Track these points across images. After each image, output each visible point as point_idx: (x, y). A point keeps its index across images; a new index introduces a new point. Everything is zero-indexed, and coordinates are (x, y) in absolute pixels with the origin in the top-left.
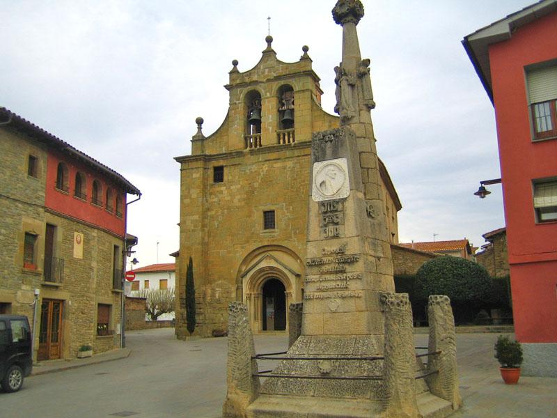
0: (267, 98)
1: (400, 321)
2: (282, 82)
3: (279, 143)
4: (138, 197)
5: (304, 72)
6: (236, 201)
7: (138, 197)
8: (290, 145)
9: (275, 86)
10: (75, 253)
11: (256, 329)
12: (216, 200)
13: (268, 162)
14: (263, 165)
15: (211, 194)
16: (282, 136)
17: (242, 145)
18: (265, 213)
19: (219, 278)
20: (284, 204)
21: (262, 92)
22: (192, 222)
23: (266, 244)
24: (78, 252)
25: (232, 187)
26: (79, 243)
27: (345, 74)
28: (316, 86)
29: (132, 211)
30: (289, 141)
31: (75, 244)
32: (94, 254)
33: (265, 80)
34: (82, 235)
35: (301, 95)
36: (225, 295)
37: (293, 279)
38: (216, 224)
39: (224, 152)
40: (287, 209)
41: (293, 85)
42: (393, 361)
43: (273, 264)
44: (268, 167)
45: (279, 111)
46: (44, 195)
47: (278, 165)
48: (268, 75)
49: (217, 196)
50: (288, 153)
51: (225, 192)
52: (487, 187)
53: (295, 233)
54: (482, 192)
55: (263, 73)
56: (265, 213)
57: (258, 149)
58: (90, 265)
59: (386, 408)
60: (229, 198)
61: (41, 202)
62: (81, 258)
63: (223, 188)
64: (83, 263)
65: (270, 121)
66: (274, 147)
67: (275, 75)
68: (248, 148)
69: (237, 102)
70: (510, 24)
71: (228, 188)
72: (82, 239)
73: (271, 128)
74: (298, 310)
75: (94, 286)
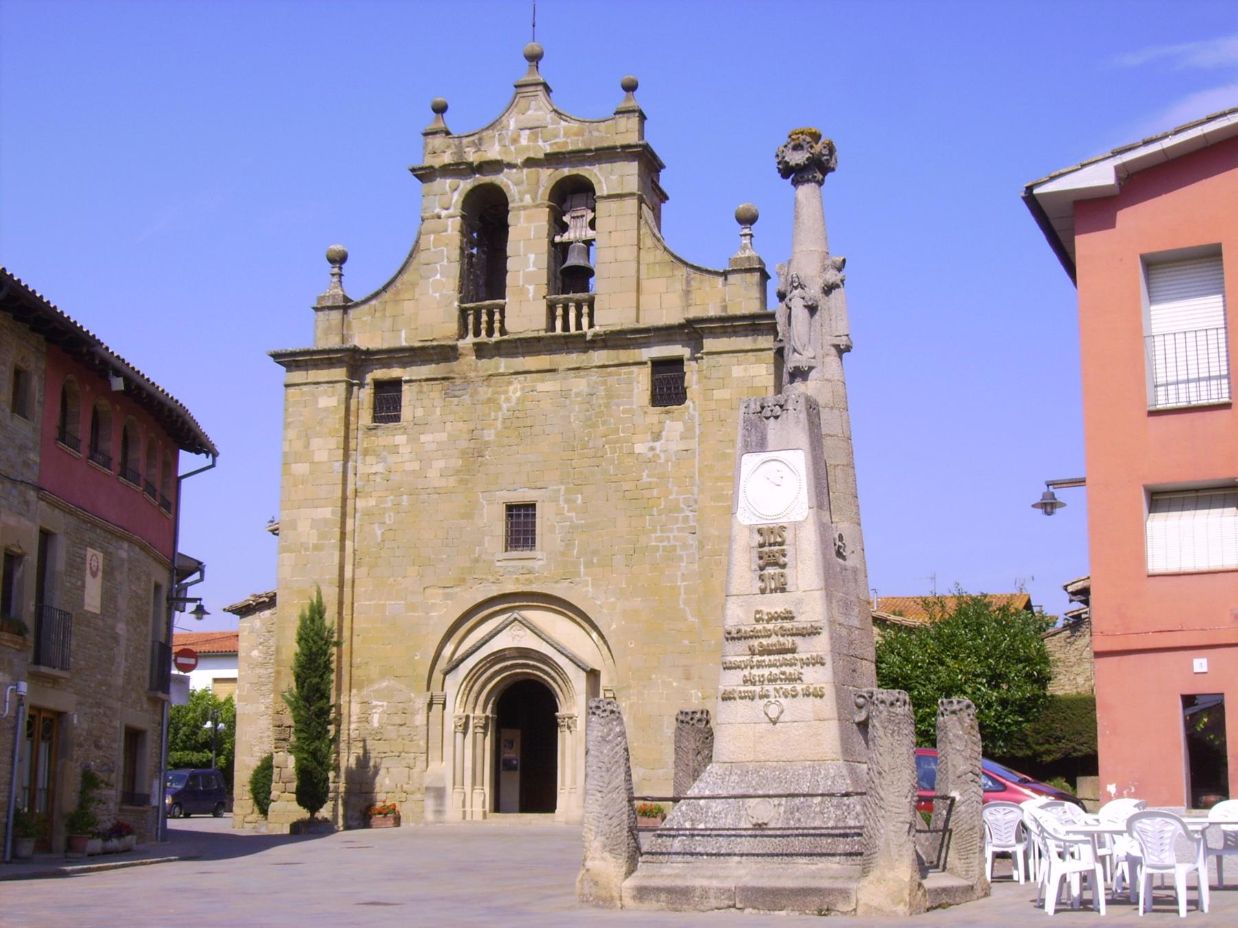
0: (525, 208)
1: (894, 731)
2: (566, 171)
3: (553, 329)
4: (209, 461)
5: (624, 147)
6: (433, 473)
7: (209, 461)
8: (584, 335)
9: (548, 177)
10: (88, 600)
11: (478, 809)
12: (379, 468)
13: (521, 377)
14: (510, 383)
15: (366, 452)
16: (559, 311)
17: (453, 327)
18: (510, 508)
19: (383, 676)
20: (563, 488)
21: (512, 191)
22: (315, 523)
23: (510, 588)
24: (93, 599)
25: (423, 438)
26: (94, 575)
27: (801, 286)
28: (653, 181)
29: (191, 495)
30: (579, 326)
31: (89, 578)
32: (122, 603)
33: (519, 161)
34: (100, 556)
35: (614, 205)
36: (397, 720)
37: (579, 681)
38: (379, 532)
39: (404, 344)
40: (567, 501)
41: (594, 181)
42: (882, 794)
43: (529, 641)
44: (523, 389)
45: (553, 244)
46: (38, 460)
47: (548, 385)
48: (527, 148)
49: (384, 460)
50: (574, 359)
51: (405, 450)
52: (1060, 494)
53: (589, 565)
54: (1049, 505)
55: (515, 141)
56: (510, 508)
57: (497, 343)
58: (113, 628)
59: (869, 872)
60: (416, 466)
61: (32, 476)
62: (98, 611)
63: (400, 439)
64: (100, 623)
65: (532, 269)
66: (539, 339)
67: (548, 151)
68: (470, 339)
69: (444, 213)
70: (1118, 169)
71: (413, 440)
72: (101, 567)
73: (531, 288)
74: (694, 721)
75: (120, 681)
